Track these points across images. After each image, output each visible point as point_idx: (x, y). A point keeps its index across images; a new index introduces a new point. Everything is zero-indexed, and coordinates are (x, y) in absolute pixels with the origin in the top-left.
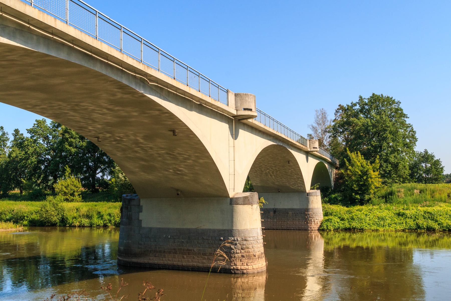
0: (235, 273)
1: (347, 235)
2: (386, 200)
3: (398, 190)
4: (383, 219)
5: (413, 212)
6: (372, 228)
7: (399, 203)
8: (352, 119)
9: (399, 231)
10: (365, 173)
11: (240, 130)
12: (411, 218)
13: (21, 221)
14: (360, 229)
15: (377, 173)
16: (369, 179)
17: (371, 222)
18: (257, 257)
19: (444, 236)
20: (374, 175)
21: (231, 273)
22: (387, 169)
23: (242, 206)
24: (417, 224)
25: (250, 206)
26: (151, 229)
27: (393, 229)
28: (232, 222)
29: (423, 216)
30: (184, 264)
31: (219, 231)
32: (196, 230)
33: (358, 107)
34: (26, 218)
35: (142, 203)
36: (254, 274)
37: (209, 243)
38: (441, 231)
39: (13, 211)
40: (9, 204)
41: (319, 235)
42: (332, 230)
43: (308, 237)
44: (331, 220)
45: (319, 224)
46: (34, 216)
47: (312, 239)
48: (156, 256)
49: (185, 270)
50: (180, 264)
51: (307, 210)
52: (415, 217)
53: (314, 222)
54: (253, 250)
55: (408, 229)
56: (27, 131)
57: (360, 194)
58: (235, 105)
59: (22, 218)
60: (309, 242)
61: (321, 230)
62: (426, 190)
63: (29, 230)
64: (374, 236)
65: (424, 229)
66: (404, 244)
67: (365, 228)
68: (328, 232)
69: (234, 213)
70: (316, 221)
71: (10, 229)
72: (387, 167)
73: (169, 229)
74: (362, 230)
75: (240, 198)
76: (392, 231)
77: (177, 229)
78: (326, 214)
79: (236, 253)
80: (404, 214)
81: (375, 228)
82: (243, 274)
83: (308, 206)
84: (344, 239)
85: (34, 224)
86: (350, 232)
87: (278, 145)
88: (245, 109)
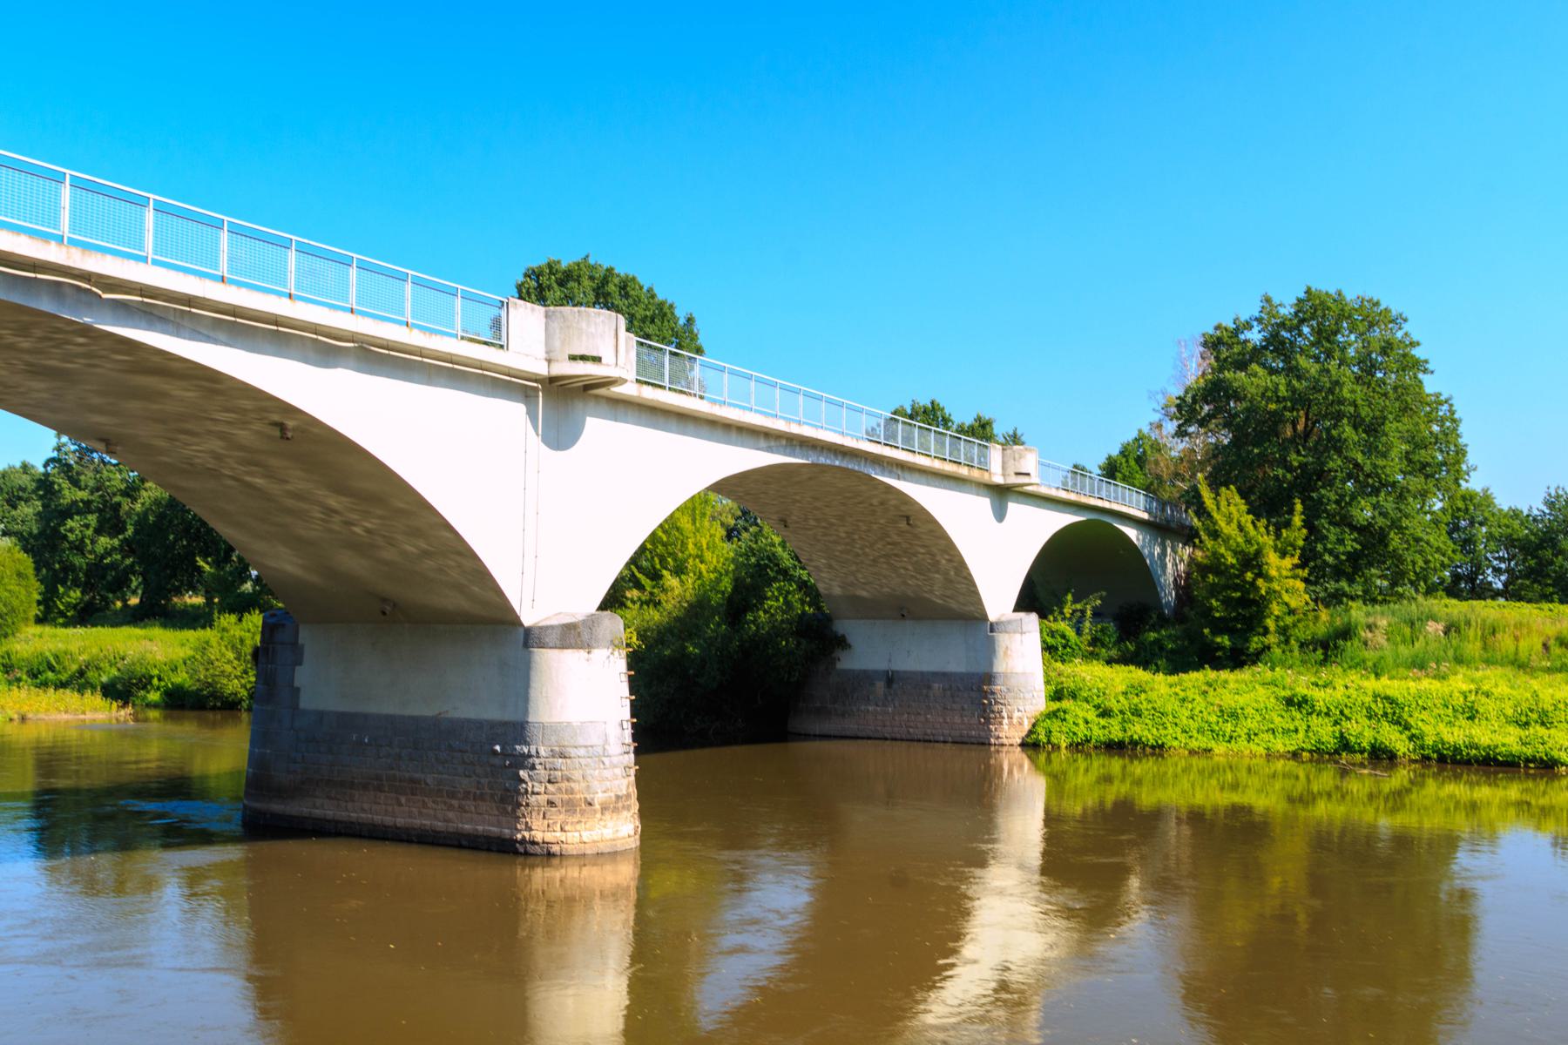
0: (526, 854)
1: (1116, 764)
2: (1325, 654)
3: (1371, 620)
4: (1234, 715)
5: (1340, 694)
6: (1194, 744)
7: (1360, 664)
8: (1228, 375)
9: (1281, 756)
10: (1252, 561)
11: (589, 420)
12: (1327, 714)
13: (142, 693)
14: (1153, 747)
15: (1288, 562)
16: (1260, 582)
17: (1193, 725)
18: (597, 807)
19: (1423, 776)
20: (1277, 565)
21: (516, 853)
22: (1341, 549)
23: (556, 652)
24: (1342, 734)
25: (582, 653)
26: (321, 715)
27: (1261, 750)
29: (1369, 709)
30: (400, 822)
31: (493, 725)
33: (1255, 336)
34: (155, 681)
35: (305, 636)
36: (582, 859)
37: (464, 762)
38: (1415, 761)
41: (1026, 763)
42: (1064, 745)
43: (988, 766)
45: (1027, 726)
48: (330, 798)
49: (401, 841)
50: (388, 820)
51: (989, 678)
52: (1342, 712)
53: (1010, 718)
54: (583, 785)
55: (1311, 751)
56: (1430, 367)
57: (1231, 632)
59: (145, 682)
61: (1031, 745)
62: (1468, 623)
64: (1201, 772)
65: (1362, 751)
66: (1301, 799)
67: (1170, 742)
68: (1049, 754)
69: (533, 673)
70: (1016, 715)
71: (89, 716)
72: (1341, 541)
73: (366, 716)
74: (1158, 750)
75: (552, 627)
76: (1253, 755)
78: (1057, 696)
80: (1306, 702)
81: (1203, 745)
82: (548, 856)
83: (991, 664)
84: (1107, 779)
85: (179, 702)
86: (1122, 756)
87: (813, 465)
88: (573, 358)
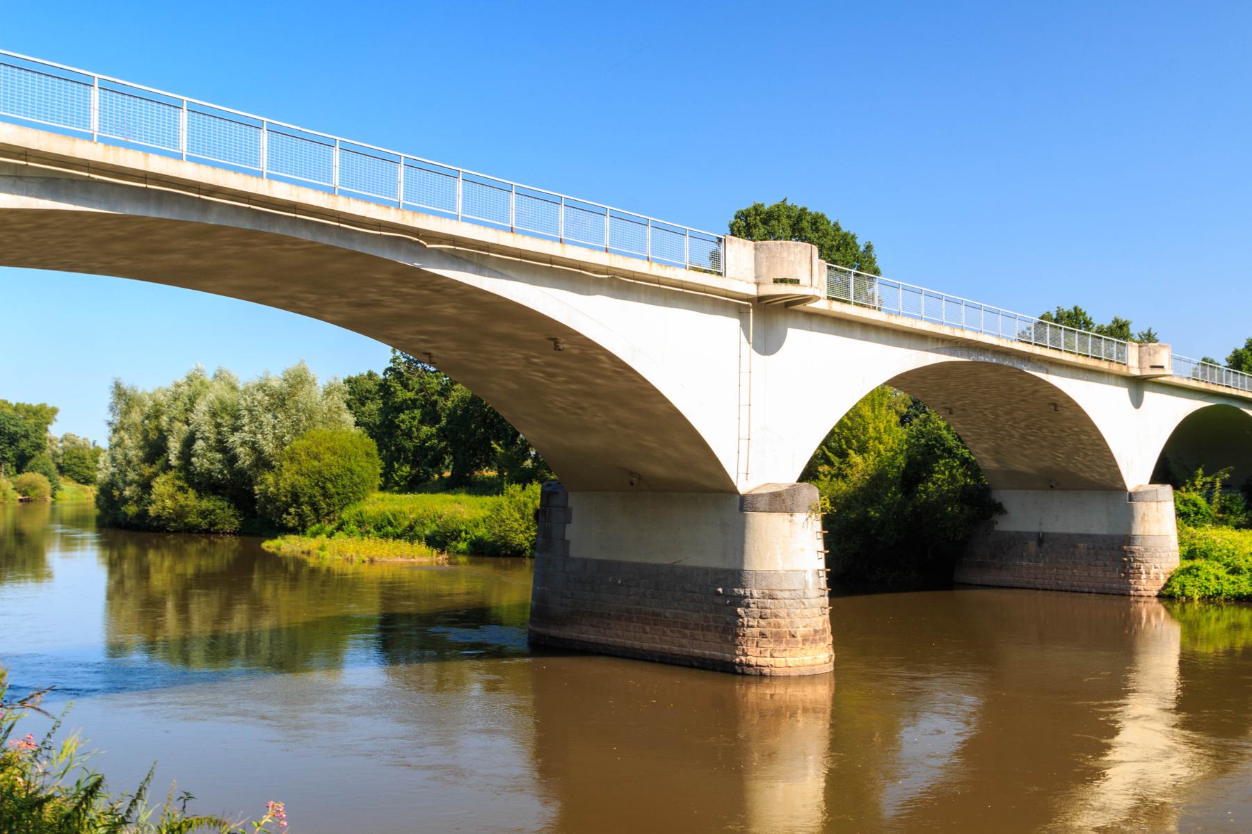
0: (743, 674)
13: (454, 543)
25: (786, 516)
26: (585, 562)
28: (742, 552)
30: (646, 645)
31: (716, 571)
32: (672, 568)
34: (463, 534)
39: (440, 517)
40: (445, 501)
41: (1163, 612)
42: (1197, 597)
43: (1128, 615)
44: (1197, 569)
45: (1163, 580)
46: (481, 532)
47: (1140, 623)
48: (592, 626)
51: (1128, 539)
53: (1148, 573)
58: (756, 271)
59: (456, 535)
60: (1130, 630)
61: (1166, 597)
63: (471, 562)
68: (1183, 604)
70: (1153, 571)
71: (417, 560)
73: (619, 563)
77: (635, 564)
78: (1190, 555)
79: (748, 626)
82: (760, 676)
83: (1130, 528)
87: (974, 363)
